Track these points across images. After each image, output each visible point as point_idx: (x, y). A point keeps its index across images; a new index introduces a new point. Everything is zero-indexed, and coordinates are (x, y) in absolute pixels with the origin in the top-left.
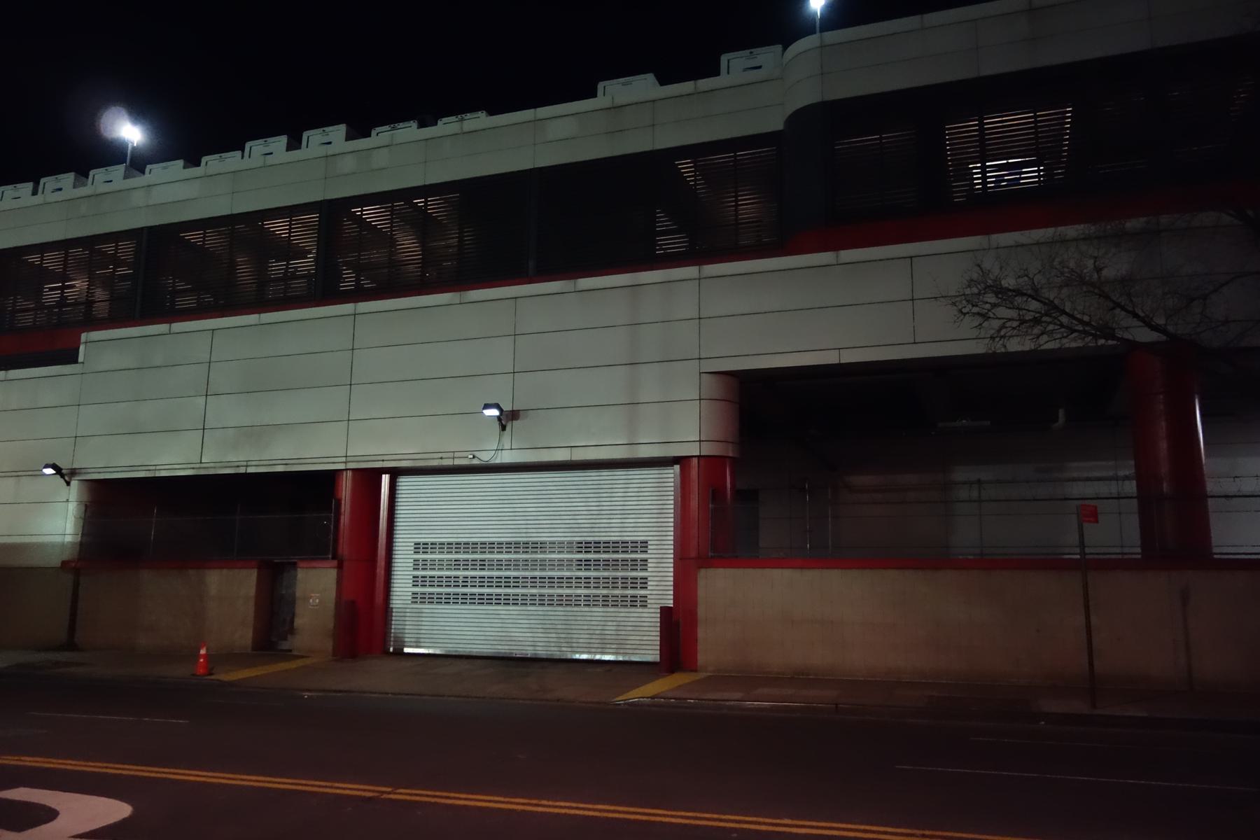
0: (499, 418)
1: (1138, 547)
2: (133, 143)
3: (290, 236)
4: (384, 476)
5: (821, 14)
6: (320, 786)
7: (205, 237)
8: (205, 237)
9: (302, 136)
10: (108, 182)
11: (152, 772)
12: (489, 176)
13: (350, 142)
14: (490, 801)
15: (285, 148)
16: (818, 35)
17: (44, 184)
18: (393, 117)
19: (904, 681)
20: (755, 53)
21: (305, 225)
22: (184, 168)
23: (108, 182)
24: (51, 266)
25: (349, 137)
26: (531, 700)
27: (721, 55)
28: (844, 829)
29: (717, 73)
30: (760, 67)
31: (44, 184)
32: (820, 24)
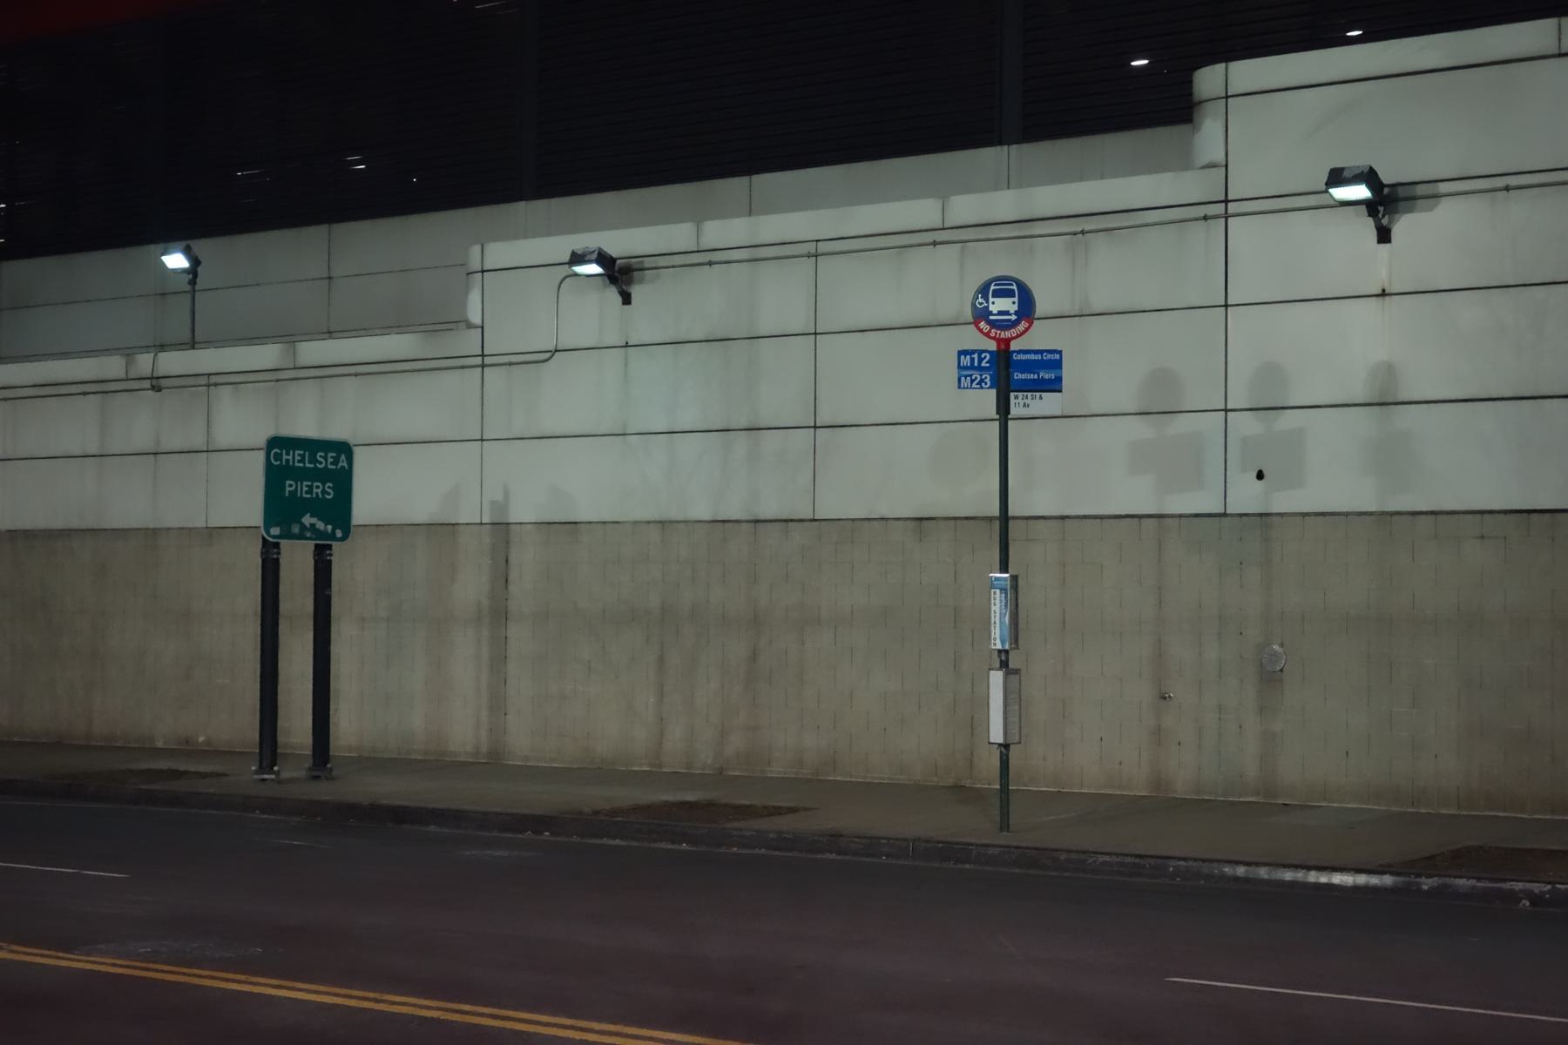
0: (1371, 207)
4: (278, 529)
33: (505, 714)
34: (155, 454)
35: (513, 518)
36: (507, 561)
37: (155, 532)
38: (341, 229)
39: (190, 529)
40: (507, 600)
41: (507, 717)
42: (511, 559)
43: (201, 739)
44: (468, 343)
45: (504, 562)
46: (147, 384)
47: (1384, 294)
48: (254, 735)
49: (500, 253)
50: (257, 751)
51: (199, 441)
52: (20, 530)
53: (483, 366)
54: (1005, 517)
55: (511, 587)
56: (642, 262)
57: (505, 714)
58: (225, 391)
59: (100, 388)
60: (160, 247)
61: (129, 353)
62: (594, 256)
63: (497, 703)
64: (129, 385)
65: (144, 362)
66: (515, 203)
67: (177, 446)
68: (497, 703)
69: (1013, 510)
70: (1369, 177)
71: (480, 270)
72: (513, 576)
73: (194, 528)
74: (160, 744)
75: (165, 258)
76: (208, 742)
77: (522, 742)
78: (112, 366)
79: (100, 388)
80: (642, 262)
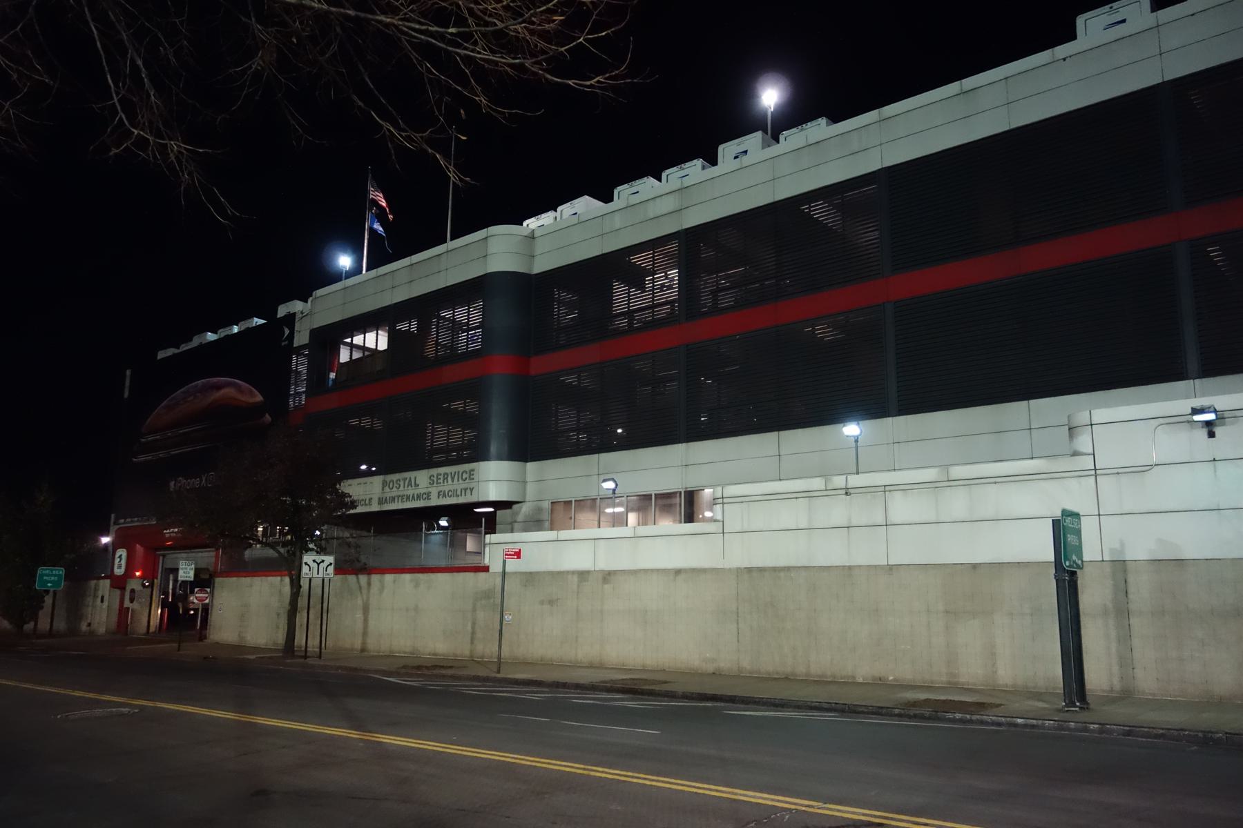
1: (358, 578)
2: (345, 268)
3: (469, 321)
5: (349, 268)
6: (710, 790)
7: (654, 256)
8: (654, 256)
9: (277, 309)
10: (635, 193)
11: (429, 745)
12: (594, 257)
13: (780, 142)
14: (422, 744)
15: (1149, 10)
16: (343, 281)
17: (561, 211)
18: (679, 159)
19: (798, 678)
20: (1114, 8)
21: (665, 255)
22: (703, 168)
23: (635, 193)
24: (643, 263)
25: (766, 145)
26: (1149, 728)
27: (158, 351)
28: (729, 793)
29: (1072, 36)
30: (1124, 21)
31: (561, 211)
32: (772, 120)
33: (1133, 668)
34: (848, 527)
35: (1129, 556)
36: (1126, 581)
37: (850, 568)
38: (783, 433)
39: (876, 566)
40: (1128, 603)
41: (1135, 670)
42: (1128, 580)
43: (891, 678)
44: (1087, 462)
45: (1124, 582)
46: (844, 492)
47: (1214, 460)
48: (1056, 670)
49: (1100, 415)
50: (1063, 692)
51: (880, 519)
52: (1228, 559)
53: (723, 503)
54: (504, 573)
55: (1130, 596)
56: (1223, 414)
57: (1133, 668)
58: (898, 495)
59: (808, 495)
60: (842, 425)
61: (826, 476)
62: (1212, 409)
63: (1126, 662)
64: (828, 492)
65: (839, 481)
66: (885, 419)
67: (863, 522)
68: (1126, 662)
69: (507, 570)
70: (1215, 411)
71: (1032, 430)
72: (1131, 589)
73: (879, 565)
74: (861, 680)
75: (259, 398)
76: (895, 680)
77: (1147, 681)
78: (817, 483)
79: (808, 495)
80: (1223, 414)
